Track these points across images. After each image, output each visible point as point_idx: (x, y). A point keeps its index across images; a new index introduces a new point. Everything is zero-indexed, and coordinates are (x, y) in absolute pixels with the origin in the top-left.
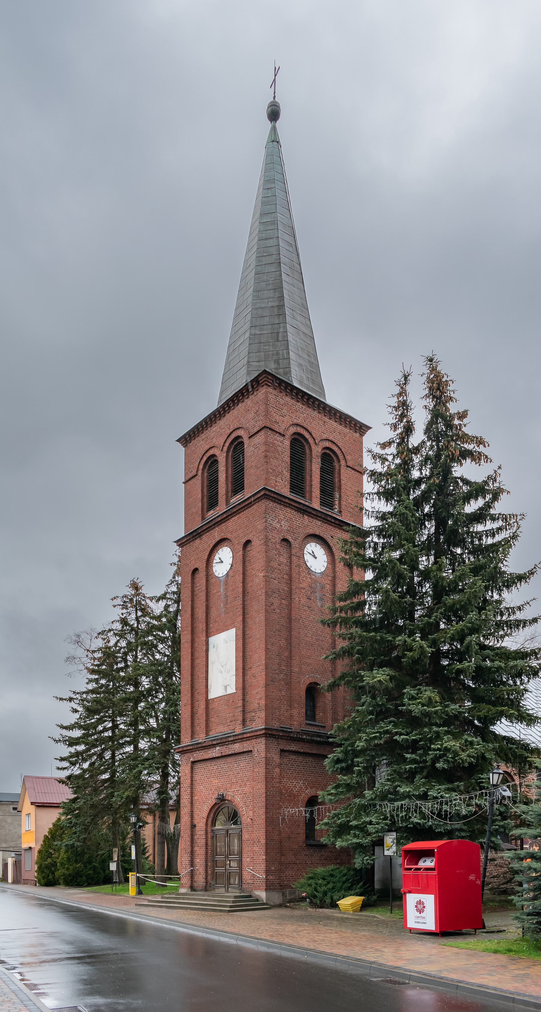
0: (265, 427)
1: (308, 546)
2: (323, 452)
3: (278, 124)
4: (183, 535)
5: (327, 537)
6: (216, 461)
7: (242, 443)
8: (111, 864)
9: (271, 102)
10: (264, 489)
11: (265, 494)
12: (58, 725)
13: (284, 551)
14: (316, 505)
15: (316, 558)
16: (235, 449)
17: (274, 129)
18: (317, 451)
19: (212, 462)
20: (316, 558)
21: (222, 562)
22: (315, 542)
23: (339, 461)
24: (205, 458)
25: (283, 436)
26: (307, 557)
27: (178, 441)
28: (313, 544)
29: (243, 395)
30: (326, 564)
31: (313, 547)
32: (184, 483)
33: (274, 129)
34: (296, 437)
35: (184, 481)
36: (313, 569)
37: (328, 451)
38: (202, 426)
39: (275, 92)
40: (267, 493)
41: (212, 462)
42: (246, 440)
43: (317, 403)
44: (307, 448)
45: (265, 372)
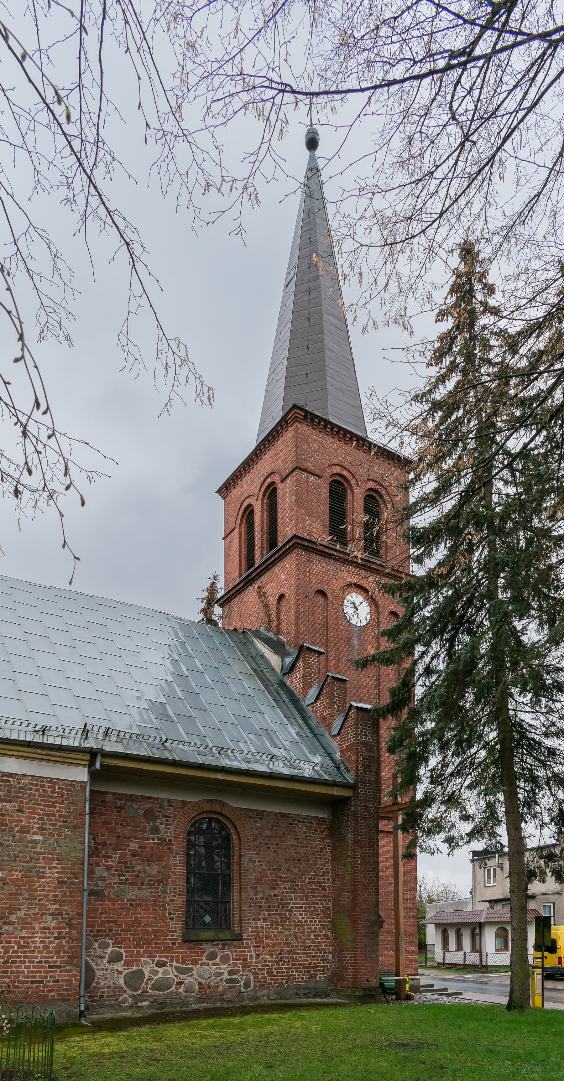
0: (297, 468)
1: (349, 597)
2: (331, 479)
3: (318, 153)
6: (252, 511)
7: (275, 489)
8: (205, 919)
10: (295, 537)
11: (296, 543)
13: (319, 599)
17: (313, 159)
19: (249, 513)
24: (265, 486)
25: (320, 477)
26: (349, 610)
28: (354, 595)
31: (355, 597)
32: (224, 539)
33: (313, 159)
35: (223, 536)
37: (338, 479)
40: (299, 541)
41: (249, 513)
42: (279, 485)
43: (336, 429)
44: (349, 492)
45: (295, 406)
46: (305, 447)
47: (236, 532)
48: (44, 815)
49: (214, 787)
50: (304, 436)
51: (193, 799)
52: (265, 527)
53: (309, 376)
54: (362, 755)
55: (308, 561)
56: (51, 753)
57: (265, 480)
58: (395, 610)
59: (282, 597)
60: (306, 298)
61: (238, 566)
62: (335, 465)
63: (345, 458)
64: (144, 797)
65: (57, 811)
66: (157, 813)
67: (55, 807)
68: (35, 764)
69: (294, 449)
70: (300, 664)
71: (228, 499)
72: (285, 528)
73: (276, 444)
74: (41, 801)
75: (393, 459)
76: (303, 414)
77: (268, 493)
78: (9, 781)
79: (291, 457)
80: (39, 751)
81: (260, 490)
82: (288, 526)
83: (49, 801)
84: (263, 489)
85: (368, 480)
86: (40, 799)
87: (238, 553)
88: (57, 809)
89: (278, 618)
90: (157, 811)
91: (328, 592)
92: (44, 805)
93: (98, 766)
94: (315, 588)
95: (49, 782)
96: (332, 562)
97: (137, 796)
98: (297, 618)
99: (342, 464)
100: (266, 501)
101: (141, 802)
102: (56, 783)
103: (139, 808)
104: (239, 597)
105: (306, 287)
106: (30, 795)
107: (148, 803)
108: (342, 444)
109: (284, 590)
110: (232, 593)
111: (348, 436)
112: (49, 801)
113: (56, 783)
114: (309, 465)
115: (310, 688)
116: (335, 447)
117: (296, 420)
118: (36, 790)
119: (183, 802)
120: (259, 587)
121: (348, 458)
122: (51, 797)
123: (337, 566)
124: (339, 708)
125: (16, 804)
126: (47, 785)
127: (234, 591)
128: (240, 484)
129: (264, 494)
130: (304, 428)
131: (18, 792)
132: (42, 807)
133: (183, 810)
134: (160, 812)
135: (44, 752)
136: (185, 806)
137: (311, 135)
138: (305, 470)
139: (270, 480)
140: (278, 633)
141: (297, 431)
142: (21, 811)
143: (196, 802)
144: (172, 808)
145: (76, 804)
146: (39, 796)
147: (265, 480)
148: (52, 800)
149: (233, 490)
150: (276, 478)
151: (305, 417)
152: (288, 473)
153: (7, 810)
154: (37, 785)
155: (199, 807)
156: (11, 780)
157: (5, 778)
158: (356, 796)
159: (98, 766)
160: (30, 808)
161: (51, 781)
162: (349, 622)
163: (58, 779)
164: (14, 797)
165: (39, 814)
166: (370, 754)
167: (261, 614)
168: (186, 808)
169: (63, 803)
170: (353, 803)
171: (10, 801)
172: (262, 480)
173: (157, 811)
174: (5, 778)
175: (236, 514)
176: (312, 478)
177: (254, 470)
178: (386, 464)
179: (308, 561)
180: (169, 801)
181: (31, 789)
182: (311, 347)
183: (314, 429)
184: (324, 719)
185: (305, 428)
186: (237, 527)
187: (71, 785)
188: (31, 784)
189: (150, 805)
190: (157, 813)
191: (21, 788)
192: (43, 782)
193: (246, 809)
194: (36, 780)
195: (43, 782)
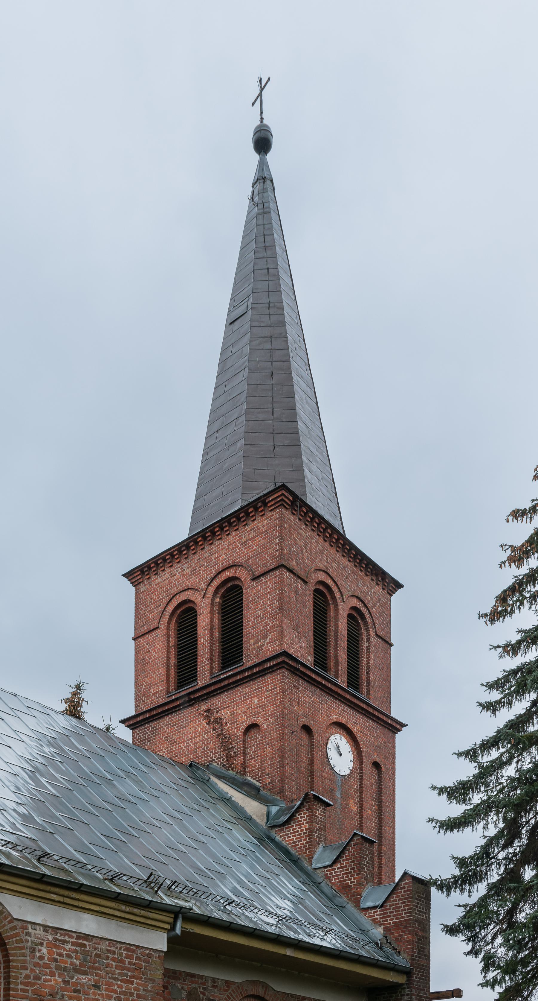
2: (315, 588)
3: (270, 157)
4: (133, 713)
5: (354, 728)
9: (259, 126)
11: (283, 662)
12: (510, 568)
13: (304, 736)
14: (342, 681)
15: (341, 755)
16: (228, 591)
17: (263, 166)
18: (344, 610)
20: (341, 755)
21: (501, 546)
22: (341, 734)
23: (368, 630)
24: (219, 580)
25: (305, 582)
26: (332, 752)
27: (124, 575)
28: (338, 736)
29: (222, 529)
30: (351, 765)
32: (134, 639)
33: (263, 166)
34: (322, 588)
35: (133, 635)
36: (336, 769)
38: (172, 556)
39: (261, 113)
40: (287, 660)
43: (323, 526)
44: (332, 607)
45: (284, 487)
46: (290, 541)
47: (161, 632)
48: (122, 993)
49: (259, 964)
50: (289, 526)
51: (237, 979)
52: (217, 634)
53: (277, 449)
54: (416, 935)
55: (295, 686)
56: (136, 911)
57: (219, 573)
58: (378, 760)
59: (253, 727)
60: (268, 346)
61: (164, 678)
62: (320, 570)
63: (329, 563)
64: (188, 974)
65: (135, 989)
66: (201, 996)
67: (132, 983)
68: (113, 924)
69: (277, 541)
70: (303, 816)
71: (143, 588)
72: (258, 641)
73: (242, 529)
74: (119, 974)
75: (377, 575)
76: (291, 499)
77: (222, 590)
78: (85, 946)
79: (271, 550)
80: (123, 907)
81: (209, 585)
82: (265, 638)
83: (126, 975)
84: (215, 584)
85: (353, 596)
86: (117, 971)
87: (164, 660)
88: (135, 985)
89: (244, 753)
90: (201, 993)
91: (314, 729)
92: (121, 981)
93: (178, 931)
94: (303, 721)
95: (127, 950)
96: (318, 692)
97: (181, 972)
98: (282, 757)
99: (328, 571)
100: (218, 600)
101: (184, 981)
102: (133, 951)
103: (182, 988)
104: (167, 719)
105: (266, 332)
106: (107, 966)
107: (192, 982)
108: (327, 545)
109: (258, 720)
110: (155, 712)
111: (336, 536)
112: (126, 975)
113: (133, 951)
114: (293, 565)
115: (317, 847)
116: (320, 547)
117: (282, 504)
118: (114, 960)
119: (227, 982)
120: (208, 711)
121: (333, 564)
122: (128, 970)
123: (323, 698)
124: (367, 876)
125: (92, 978)
126: (124, 953)
127: (160, 710)
128: (168, 570)
129: (216, 592)
130: (288, 516)
131: (95, 962)
132: (119, 983)
133: (228, 994)
134: (204, 994)
135: (128, 909)
136: (228, 987)
137: (262, 134)
138: (291, 571)
139: (230, 573)
140: (244, 773)
141: (281, 519)
142: (97, 986)
143: (241, 983)
144: (216, 990)
145: (154, 981)
146: (116, 967)
147: (219, 573)
148: (130, 974)
149: (153, 577)
150: (242, 573)
151: (293, 503)
152: (265, 569)
153: (82, 985)
154: (114, 953)
155: (243, 989)
156: (87, 943)
157: (81, 941)
158: (410, 983)
159: (178, 931)
160: (107, 984)
161: (129, 947)
162: (332, 769)
163: (137, 946)
164: (90, 968)
165: (116, 992)
166: (423, 934)
167: (212, 745)
168: (230, 991)
169: (141, 979)
170: (407, 991)
171: (85, 973)
172: (215, 573)
173: (201, 993)
174: (81, 941)
175: (161, 609)
176: (298, 583)
177: (197, 557)
178: (368, 579)
179: (295, 686)
180: (214, 980)
181: (107, 958)
182: (277, 413)
183: (300, 519)
184: (345, 888)
185: (291, 517)
186: (163, 626)
187: (149, 955)
188: (108, 950)
189: (193, 985)
190: (201, 996)
191: (97, 955)
192: (120, 948)
193: (288, 994)
194: (114, 945)
195: (120, 948)
